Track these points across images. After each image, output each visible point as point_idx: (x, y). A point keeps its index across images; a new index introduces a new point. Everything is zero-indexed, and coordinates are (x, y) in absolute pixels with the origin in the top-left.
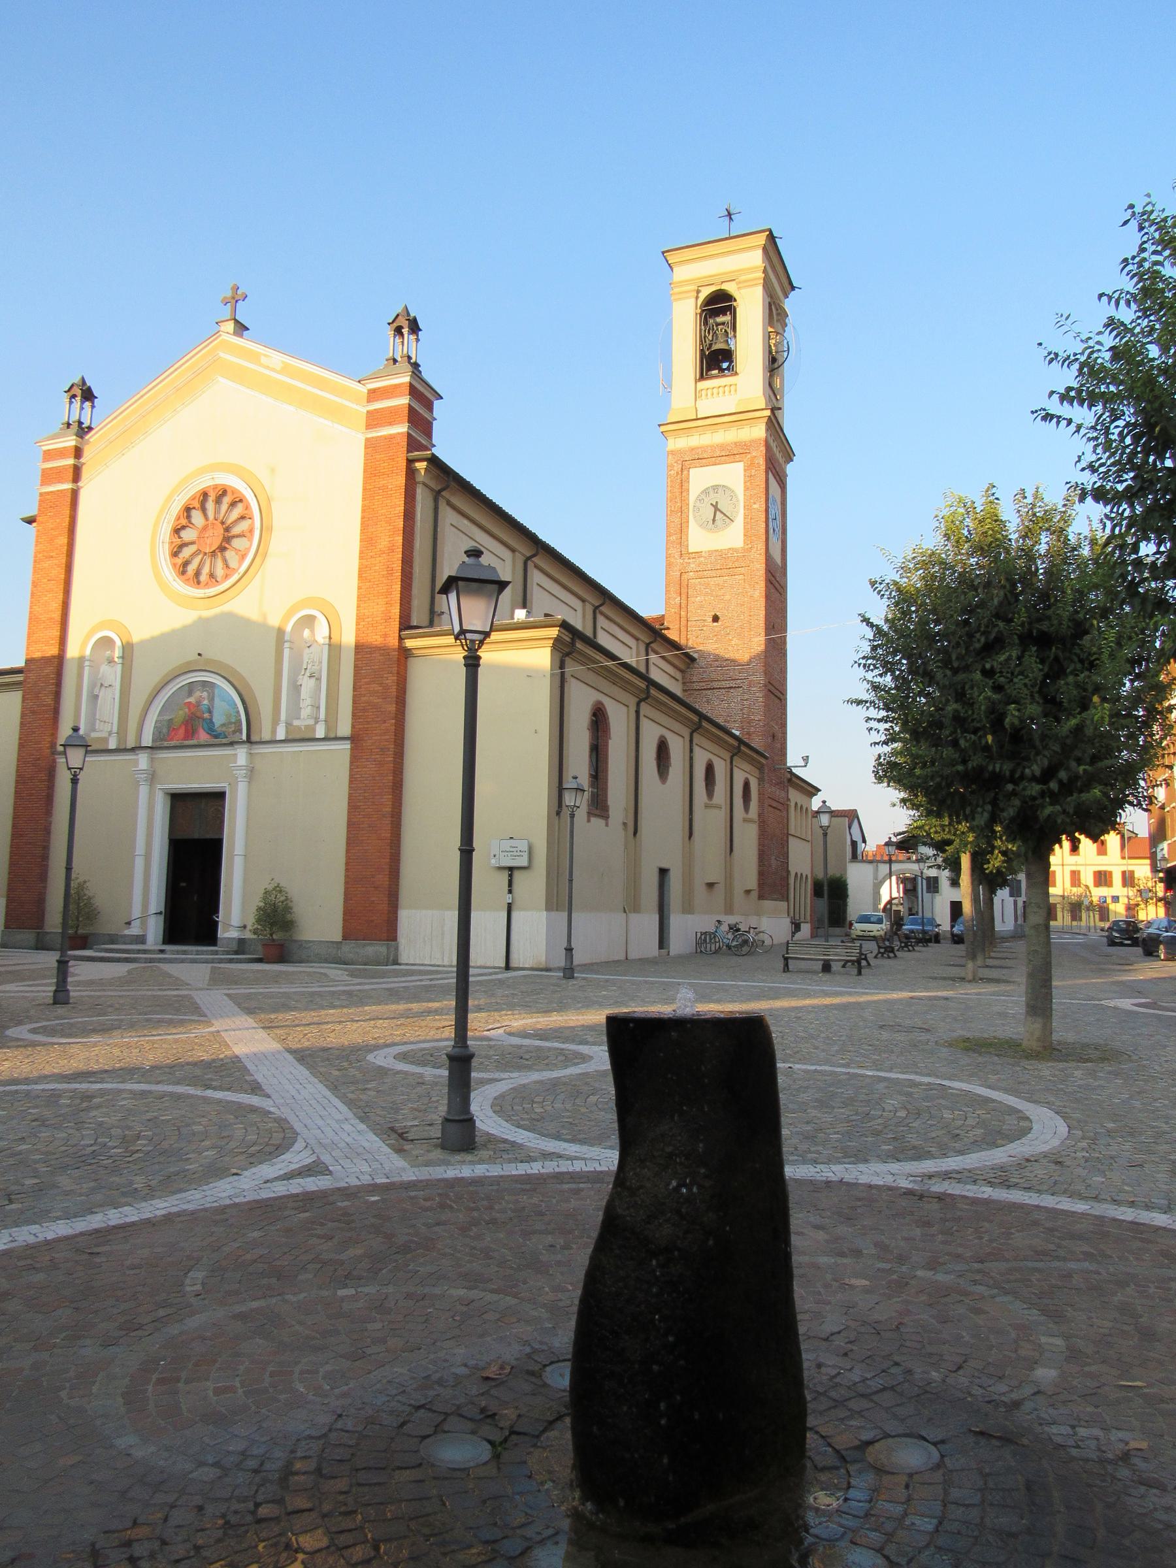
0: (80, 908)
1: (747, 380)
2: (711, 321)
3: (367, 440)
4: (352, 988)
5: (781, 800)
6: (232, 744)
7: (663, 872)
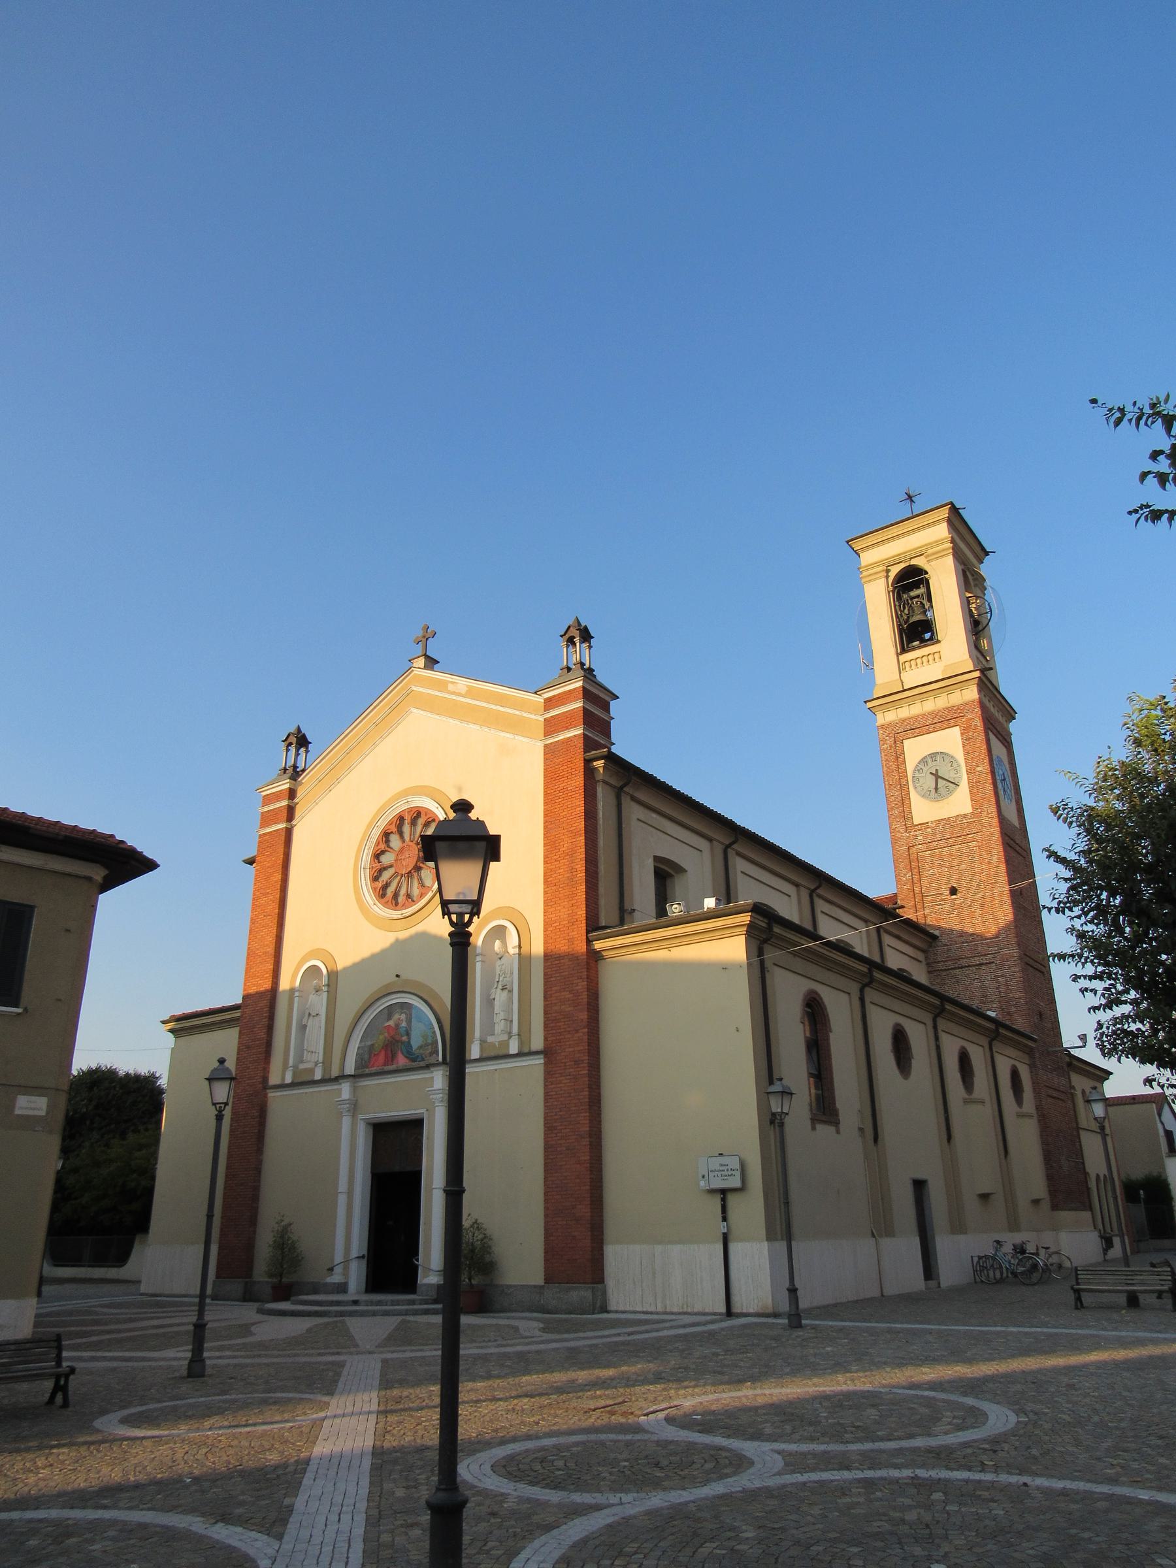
0: (287, 1252)
1: (952, 646)
2: (905, 596)
3: (546, 746)
4: (542, 1347)
5: (1062, 1088)
6: (428, 1067)
7: (919, 1185)
